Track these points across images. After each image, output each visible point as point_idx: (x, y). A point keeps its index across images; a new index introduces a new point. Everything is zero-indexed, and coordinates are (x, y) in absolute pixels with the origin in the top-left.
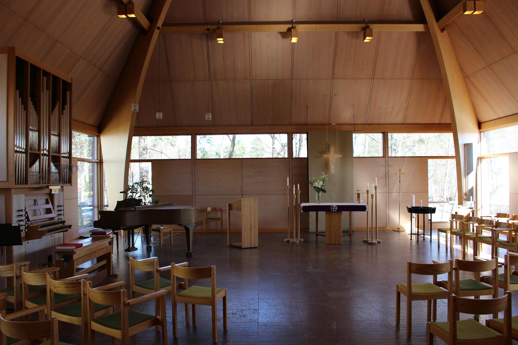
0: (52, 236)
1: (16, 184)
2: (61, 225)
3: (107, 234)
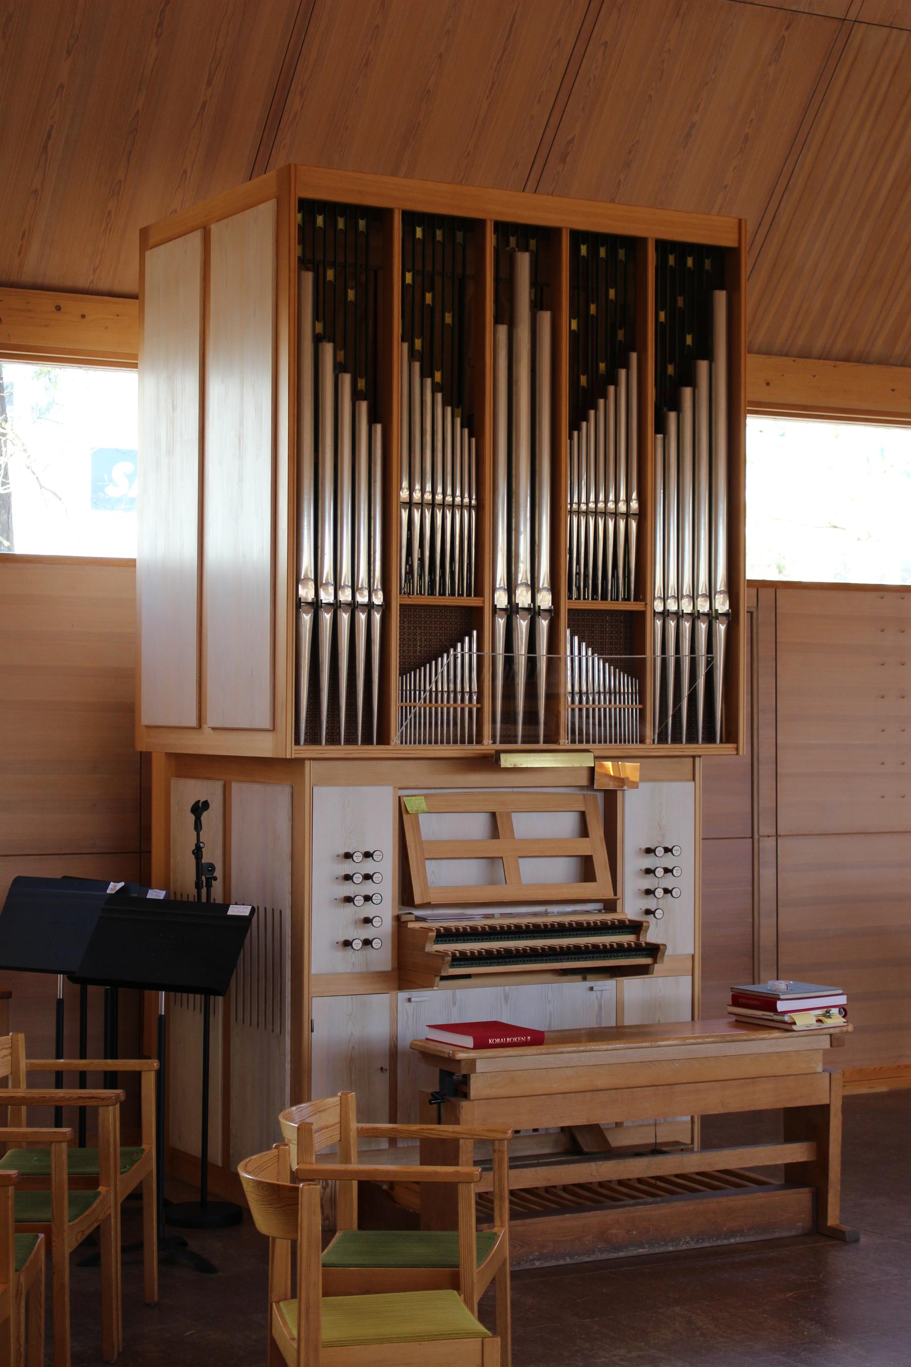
0: (591, 989)
1: (297, 742)
2: (627, 939)
3: (781, 1006)
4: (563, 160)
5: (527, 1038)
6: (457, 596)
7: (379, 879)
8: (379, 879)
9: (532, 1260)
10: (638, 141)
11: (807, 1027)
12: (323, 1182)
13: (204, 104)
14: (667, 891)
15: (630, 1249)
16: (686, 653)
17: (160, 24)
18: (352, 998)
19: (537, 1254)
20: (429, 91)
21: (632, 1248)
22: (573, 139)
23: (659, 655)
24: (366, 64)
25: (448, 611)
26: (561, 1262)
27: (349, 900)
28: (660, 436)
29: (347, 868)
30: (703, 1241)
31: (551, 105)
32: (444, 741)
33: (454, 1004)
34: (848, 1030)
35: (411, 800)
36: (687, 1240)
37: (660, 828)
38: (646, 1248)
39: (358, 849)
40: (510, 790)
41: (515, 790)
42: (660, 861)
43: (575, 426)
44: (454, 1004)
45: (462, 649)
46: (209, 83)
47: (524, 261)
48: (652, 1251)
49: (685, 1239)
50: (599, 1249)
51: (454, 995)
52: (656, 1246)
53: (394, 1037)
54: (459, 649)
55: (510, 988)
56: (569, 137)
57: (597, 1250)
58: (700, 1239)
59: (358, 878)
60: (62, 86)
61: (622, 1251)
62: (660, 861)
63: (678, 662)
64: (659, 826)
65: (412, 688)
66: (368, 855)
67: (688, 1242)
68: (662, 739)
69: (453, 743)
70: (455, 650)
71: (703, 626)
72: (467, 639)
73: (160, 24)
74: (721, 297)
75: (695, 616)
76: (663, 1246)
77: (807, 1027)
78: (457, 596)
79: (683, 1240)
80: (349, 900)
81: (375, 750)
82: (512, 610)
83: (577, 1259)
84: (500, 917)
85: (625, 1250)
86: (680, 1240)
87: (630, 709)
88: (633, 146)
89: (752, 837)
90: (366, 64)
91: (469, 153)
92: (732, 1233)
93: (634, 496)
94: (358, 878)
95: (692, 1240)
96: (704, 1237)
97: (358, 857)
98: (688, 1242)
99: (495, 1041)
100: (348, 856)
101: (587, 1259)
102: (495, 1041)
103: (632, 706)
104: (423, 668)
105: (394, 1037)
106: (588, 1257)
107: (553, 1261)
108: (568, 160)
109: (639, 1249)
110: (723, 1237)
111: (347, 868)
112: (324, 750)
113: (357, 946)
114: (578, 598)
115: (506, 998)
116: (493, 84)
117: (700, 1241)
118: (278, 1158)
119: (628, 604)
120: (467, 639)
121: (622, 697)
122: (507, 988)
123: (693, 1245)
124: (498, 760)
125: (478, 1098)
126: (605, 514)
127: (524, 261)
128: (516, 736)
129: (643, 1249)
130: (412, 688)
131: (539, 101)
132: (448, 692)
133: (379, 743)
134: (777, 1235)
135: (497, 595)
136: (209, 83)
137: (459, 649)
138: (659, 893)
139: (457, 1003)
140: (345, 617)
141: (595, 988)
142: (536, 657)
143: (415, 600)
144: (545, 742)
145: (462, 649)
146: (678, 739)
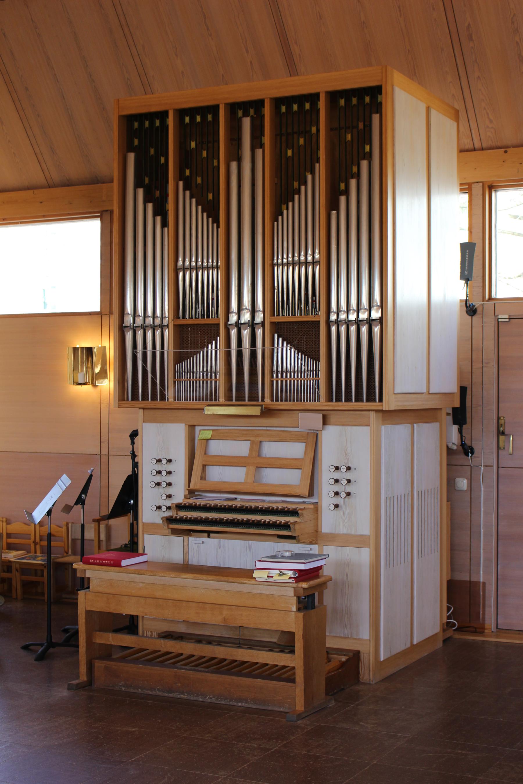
4: (470, 38)
5: (111, 562)
6: (211, 318)
7: (164, 474)
8: (164, 474)
9: (120, 686)
10: (514, 15)
11: (274, 580)
12: (150, 632)
13: (251, 62)
14: (348, 494)
15: (176, 693)
16: (158, 349)
17: (208, 29)
18: (164, 537)
19: (123, 683)
20: (364, 22)
21: (177, 693)
22: (469, 25)
23: (150, 349)
24: (321, 18)
25: (282, 325)
26: (136, 691)
27: (158, 484)
28: (334, 213)
29: (158, 467)
30: (221, 700)
31: (442, 9)
32: (287, 400)
33: (220, 548)
34: (302, 586)
35: (205, 432)
36: (211, 697)
37: (346, 455)
38: (186, 695)
39: (164, 456)
40: (265, 428)
41: (268, 428)
42: (164, 467)
43: (277, 214)
44: (220, 548)
45: (212, 348)
46: (247, 51)
47: (247, 123)
48: (189, 698)
49: (210, 696)
50: (158, 689)
51: (220, 542)
52: (191, 695)
53: (186, 561)
54: (210, 348)
55: (252, 542)
56: (467, 24)
57: (156, 689)
58: (219, 698)
59: (164, 473)
60: (182, 72)
61: (171, 694)
62: (164, 467)
63: (240, 354)
64: (345, 453)
65: (183, 371)
66: (170, 461)
67: (211, 698)
68: (330, 399)
69: (346, 401)
70: (207, 348)
71: (364, 329)
72: (214, 342)
73: (208, 29)
74: (376, 118)
75: (358, 323)
76: (196, 696)
77: (274, 580)
78: (211, 318)
79: (209, 696)
80: (158, 484)
81: (158, 404)
82: (238, 325)
83: (146, 692)
84: (251, 501)
85: (173, 693)
86: (207, 696)
87: (306, 381)
88: (512, 18)
89: (498, 467)
90: (321, 18)
91: (409, 50)
92: (241, 700)
93: (317, 251)
94: (164, 473)
95: (214, 698)
96: (222, 698)
97: (164, 461)
98: (211, 698)
99: (93, 561)
100: (159, 461)
101: (151, 693)
102: (93, 561)
103: (316, 379)
104: (189, 360)
105: (186, 561)
106: (151, 692)
107: (132, 689)
108: (473, 37)
109: (181, 695)
110: (233, 700)
111: (158, 467)
112: (343, 405)
113: (154, 509)
114: (278, 315)
115: (250, 548)
116: (399, 7)
117: (219, 699)
118: (348, 638)
119: (198, 320)
120: (214, 342)
121: (314, 373)
122: (250, 542)
123: (214, 700)
124: (262, 411)
125: (167, 598)
126: (191, 269)
127: (247, 123)
128: (244, 397)
129: (184, 695)
130: (183, 371)
131: (434, 9)
132: (193, 372)
133: (336, 401)
134: (270, 708)
135: (231, 316)
136: (247, 51)
137: (210, 348)
138: (343, 495)
139: (221, 547)
140: (364, 329)
141: (202, 542)
142: (242, 350)
143: (181, 322)
144: (249, 400)
145: (212, 348)
146: (155, 399)
